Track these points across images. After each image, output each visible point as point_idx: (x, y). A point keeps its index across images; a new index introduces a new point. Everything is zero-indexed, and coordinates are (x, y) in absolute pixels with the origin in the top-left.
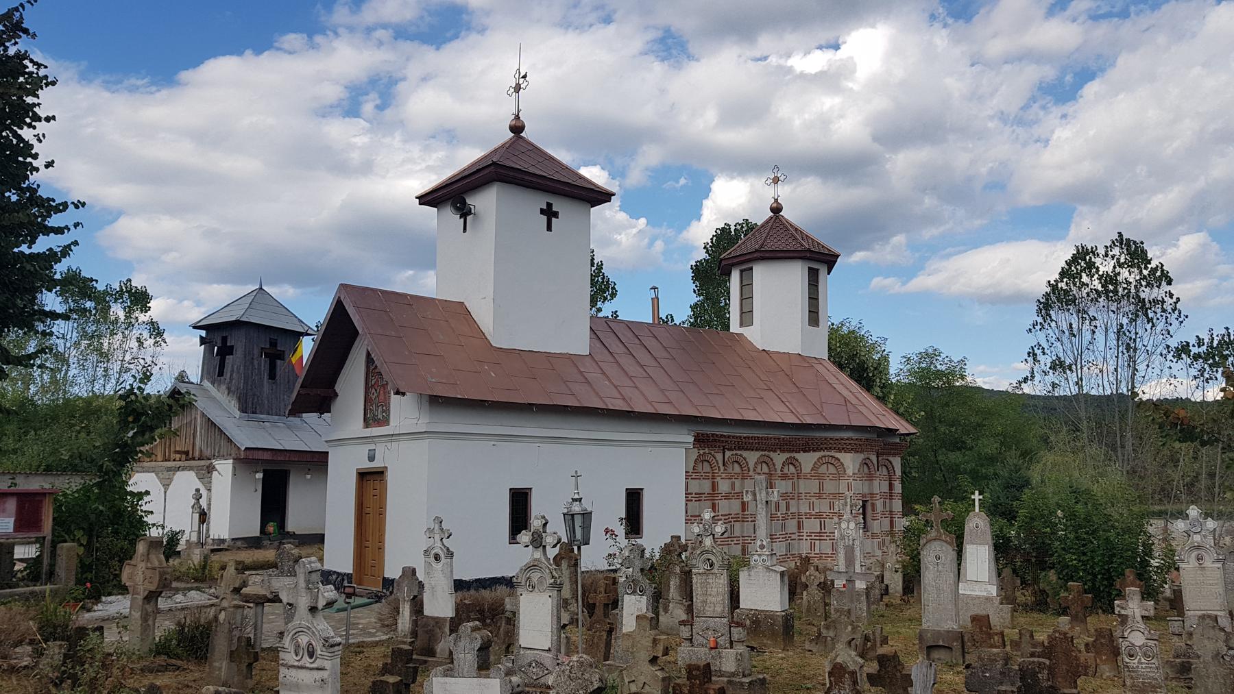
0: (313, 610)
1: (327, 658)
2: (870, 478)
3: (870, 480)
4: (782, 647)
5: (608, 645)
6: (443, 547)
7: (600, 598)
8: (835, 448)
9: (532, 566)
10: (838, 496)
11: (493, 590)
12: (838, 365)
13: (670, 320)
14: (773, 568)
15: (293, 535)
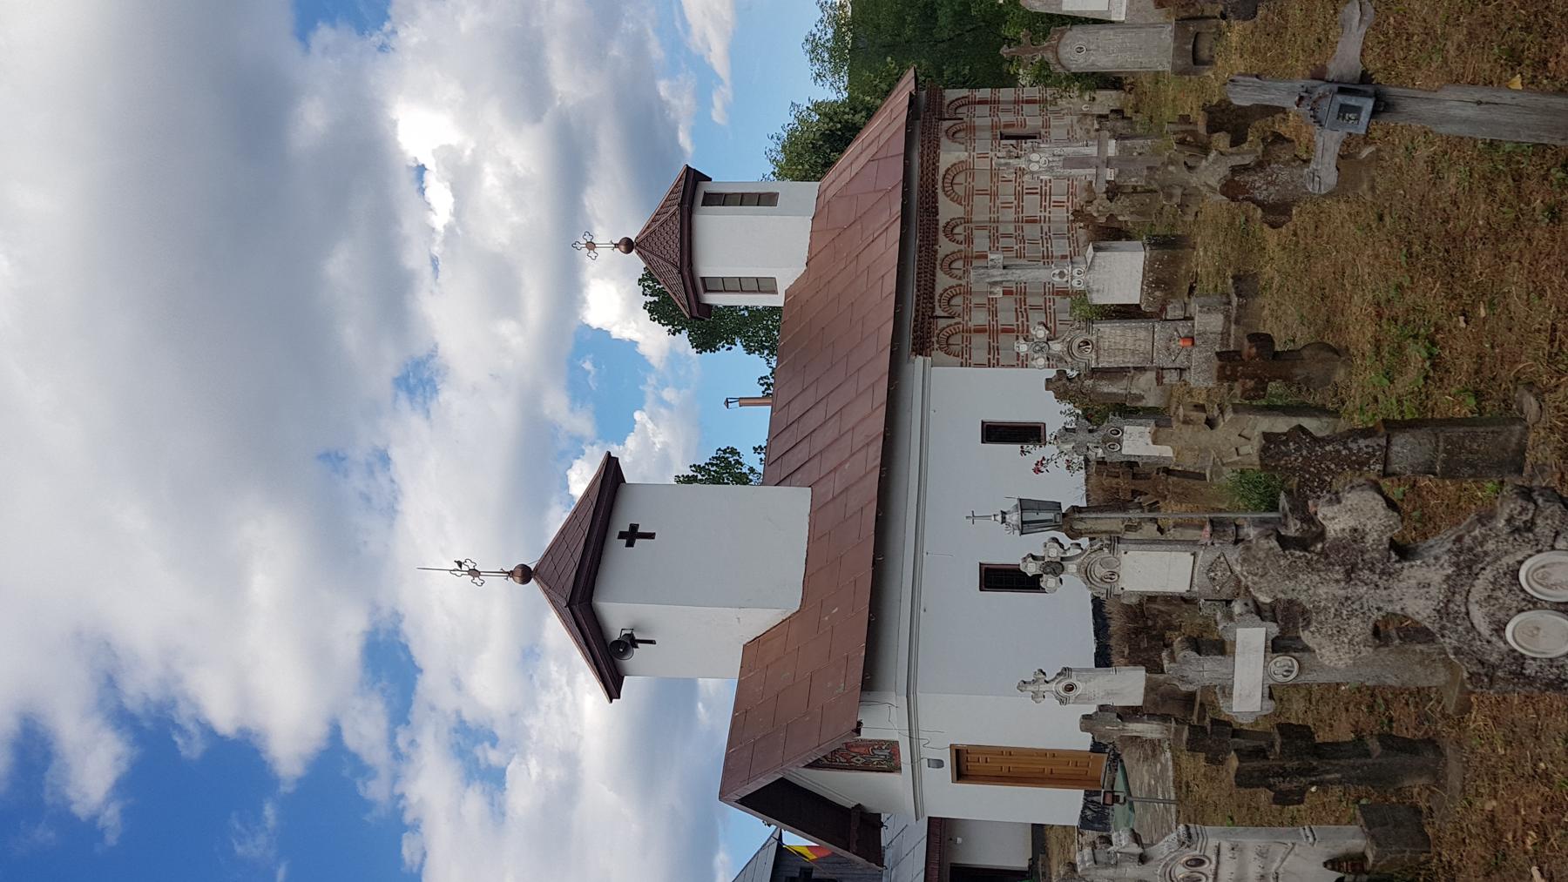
0: (1143, 859)
1: (1204, 844)
2: (972, 129)
3: (974, 129)
4: (1191, 250)
5: (1185, 474)
6: (1057, 681)
7: (1124, 483)
8: (933, 175)
9: (1087, 574)
10: (994, 173)
11: (1109, 616)
12: (826, 167)
13: (766, 381)
14: (1089, 261)
15: (1033, 861)
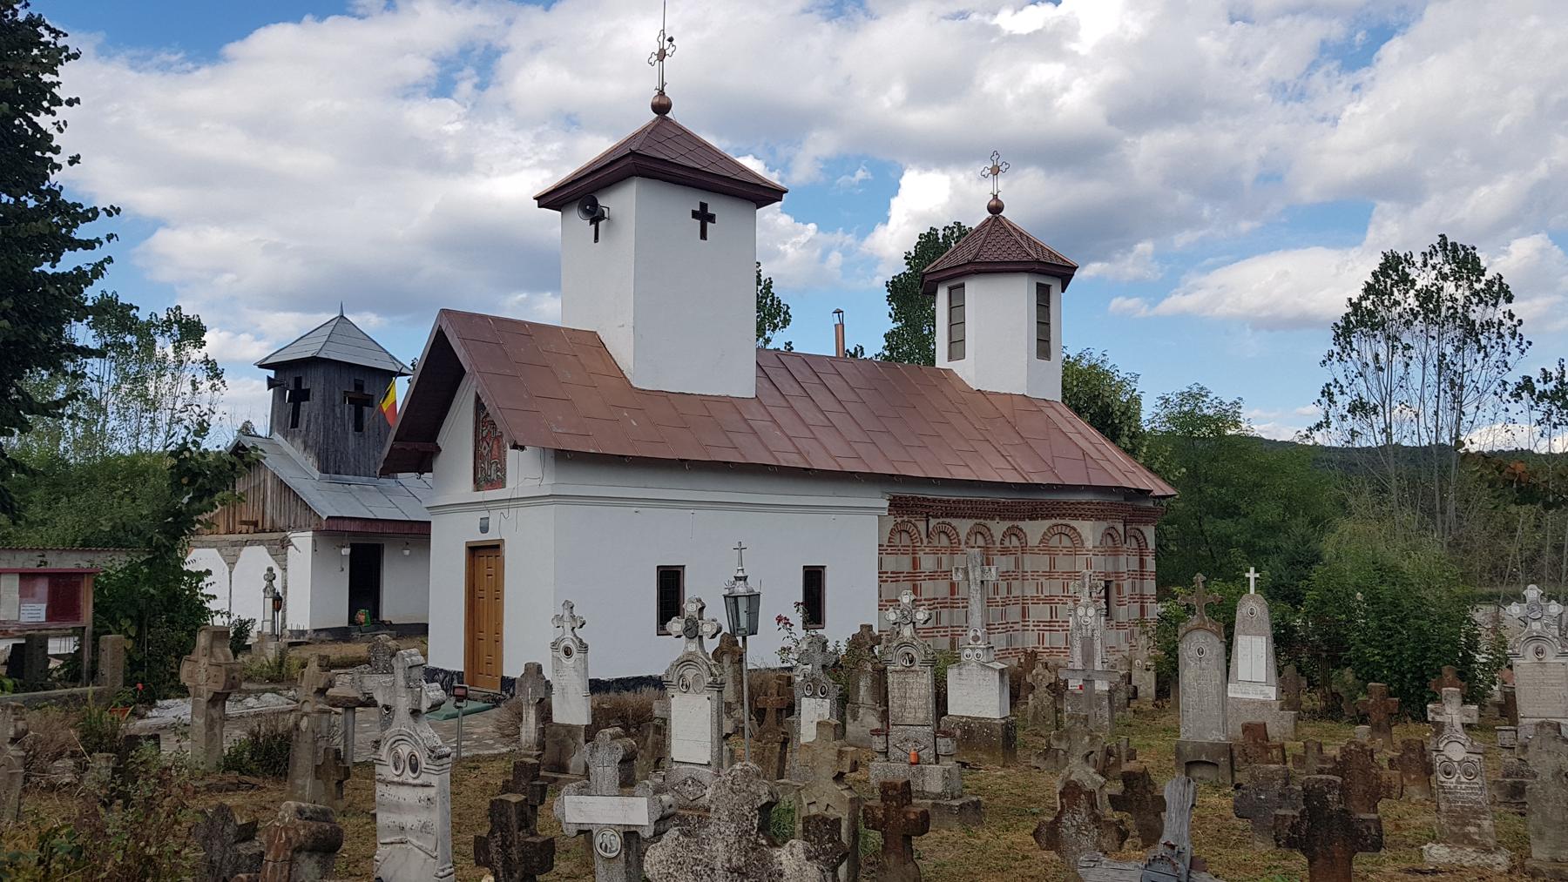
0: (415, 713)
2: (1115, 552)
5: (782, 759)
7: (772, 701)
9: (686, 662)
10: (1073, 575)
14: (990, 665)
